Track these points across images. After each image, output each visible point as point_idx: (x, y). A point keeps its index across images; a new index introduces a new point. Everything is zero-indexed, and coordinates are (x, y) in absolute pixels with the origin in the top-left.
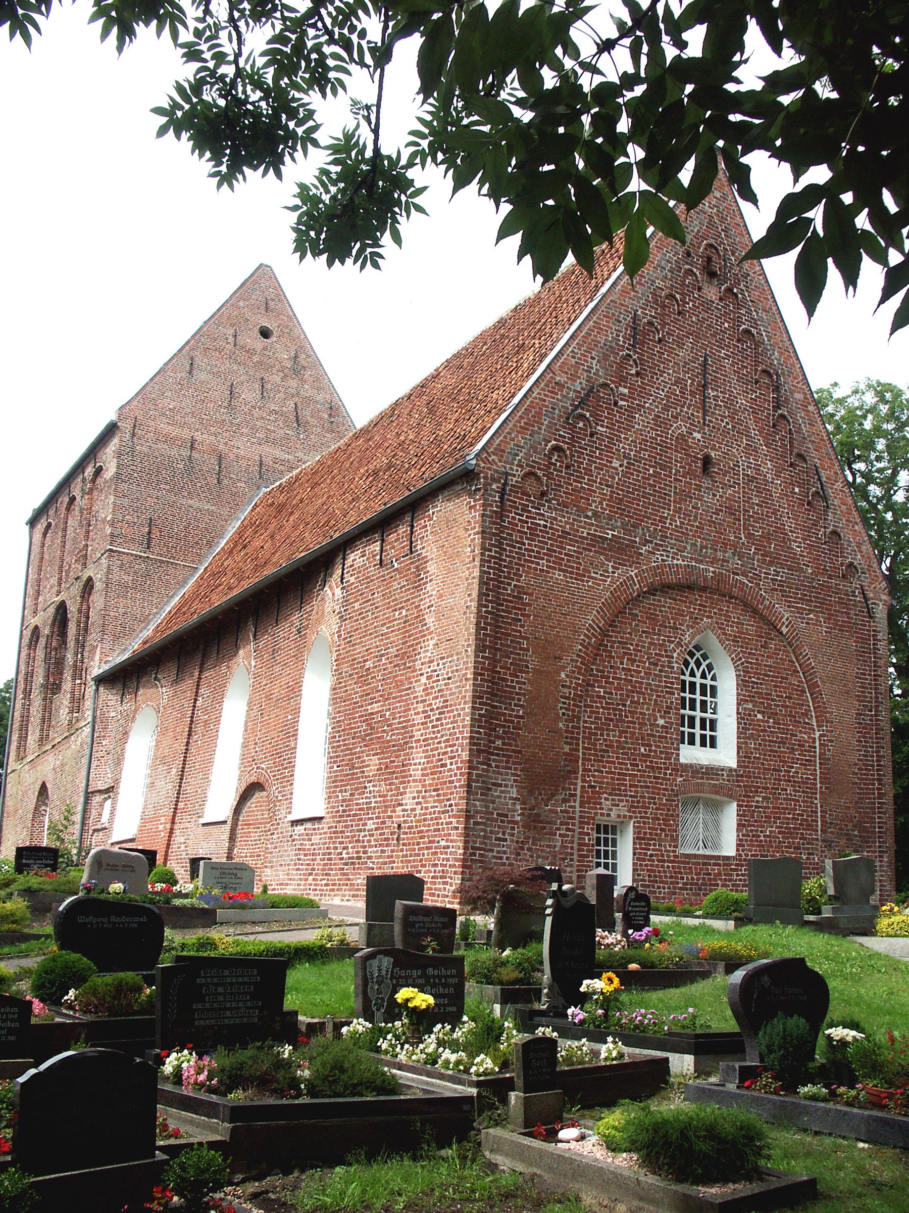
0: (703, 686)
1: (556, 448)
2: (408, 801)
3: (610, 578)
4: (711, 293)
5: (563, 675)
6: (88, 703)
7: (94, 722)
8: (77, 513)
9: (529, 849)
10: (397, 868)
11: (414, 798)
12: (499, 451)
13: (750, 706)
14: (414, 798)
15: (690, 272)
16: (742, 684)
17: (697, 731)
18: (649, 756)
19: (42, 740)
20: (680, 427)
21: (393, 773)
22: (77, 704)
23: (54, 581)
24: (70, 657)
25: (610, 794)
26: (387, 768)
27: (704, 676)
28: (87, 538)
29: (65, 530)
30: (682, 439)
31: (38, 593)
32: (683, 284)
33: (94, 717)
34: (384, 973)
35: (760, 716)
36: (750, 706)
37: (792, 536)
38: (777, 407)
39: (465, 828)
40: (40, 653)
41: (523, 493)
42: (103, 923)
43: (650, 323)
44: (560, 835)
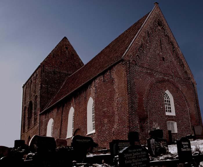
0: (167, 101)
1: (137, 55)
2: (115, 126)
3: (149, 80)
4: (160, 28)
5: (144, 99)
6: (38, 119)
7: (40, 123)
8: (33, 84)
9: (141, 133)
10: (134, 130)
11: (117, 126)
12: (128, 56)
13: (176, 104)
14: (117, 126)
15: (156, 24)
16: (174, 100)
17: (168, 109)
18: (160, 114)
19: (29, 128)
20: (158, 52)
21: (111, 122)
22: (35, 120)
23: (29, 97)
24: (33, 111)
25: (155, 122)
26: (109, 121)
27: (167, 99)
28: (35, 88)
29: (30, 87)
30: (158, 54)
31: (25, 100)
32: (155, 26)
33: (40, 122)
34: (153, 142)
35: (178, 106)
36: (176, 104)
37: (179, 72)
38: (173, 49)
39: (129, 130)
40: (27, 111)
41: (133, 64)
42: (81, 141)
43: (151, 33)
44: (147, 130)
